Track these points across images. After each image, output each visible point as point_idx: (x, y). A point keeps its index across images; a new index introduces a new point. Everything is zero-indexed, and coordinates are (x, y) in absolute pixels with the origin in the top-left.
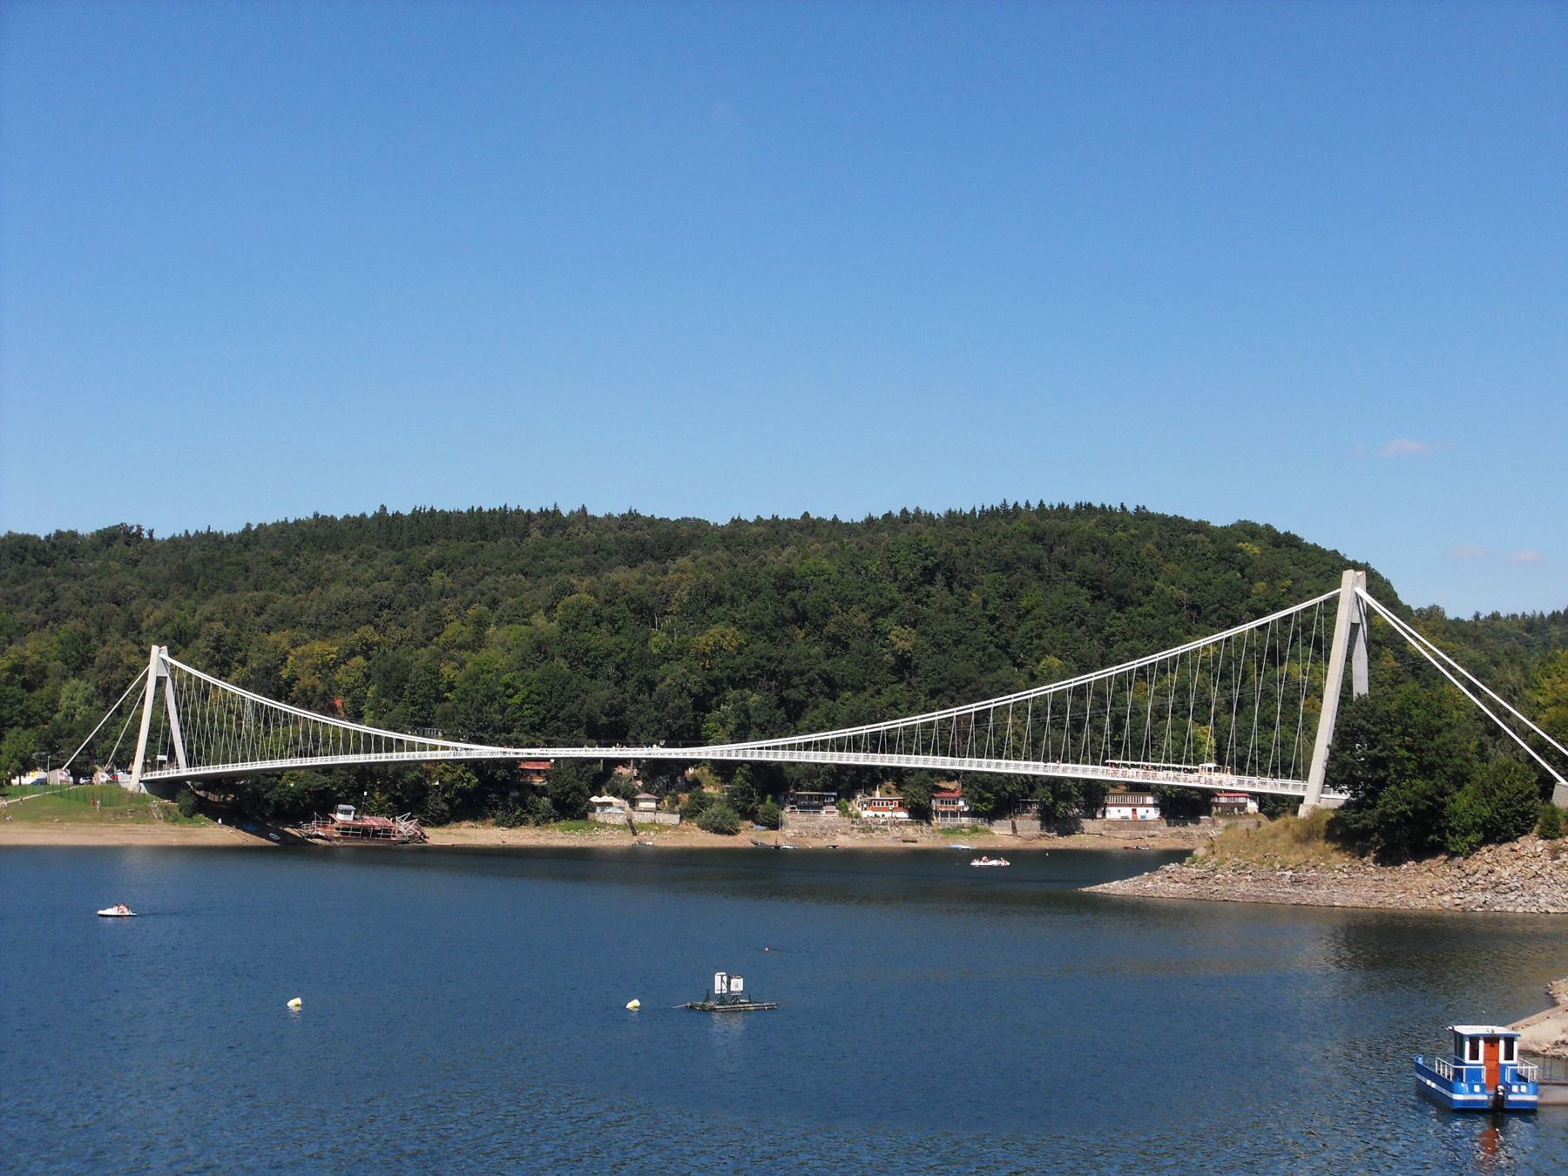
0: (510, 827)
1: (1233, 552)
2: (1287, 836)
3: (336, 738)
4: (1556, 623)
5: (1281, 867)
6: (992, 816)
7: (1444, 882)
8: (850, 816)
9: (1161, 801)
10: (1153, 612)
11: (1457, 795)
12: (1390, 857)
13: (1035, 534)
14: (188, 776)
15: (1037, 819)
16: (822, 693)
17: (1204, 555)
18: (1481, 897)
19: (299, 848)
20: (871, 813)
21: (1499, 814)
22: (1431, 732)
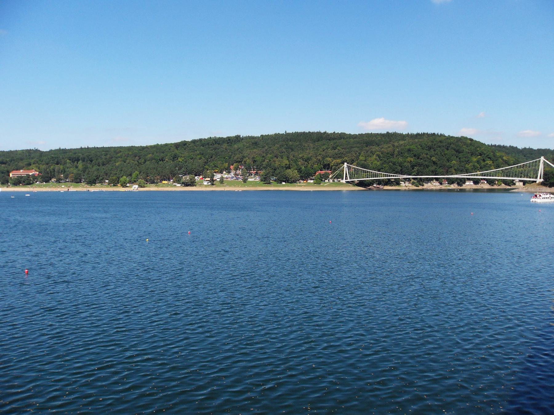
3: (375, 175)
14: (28, 192)
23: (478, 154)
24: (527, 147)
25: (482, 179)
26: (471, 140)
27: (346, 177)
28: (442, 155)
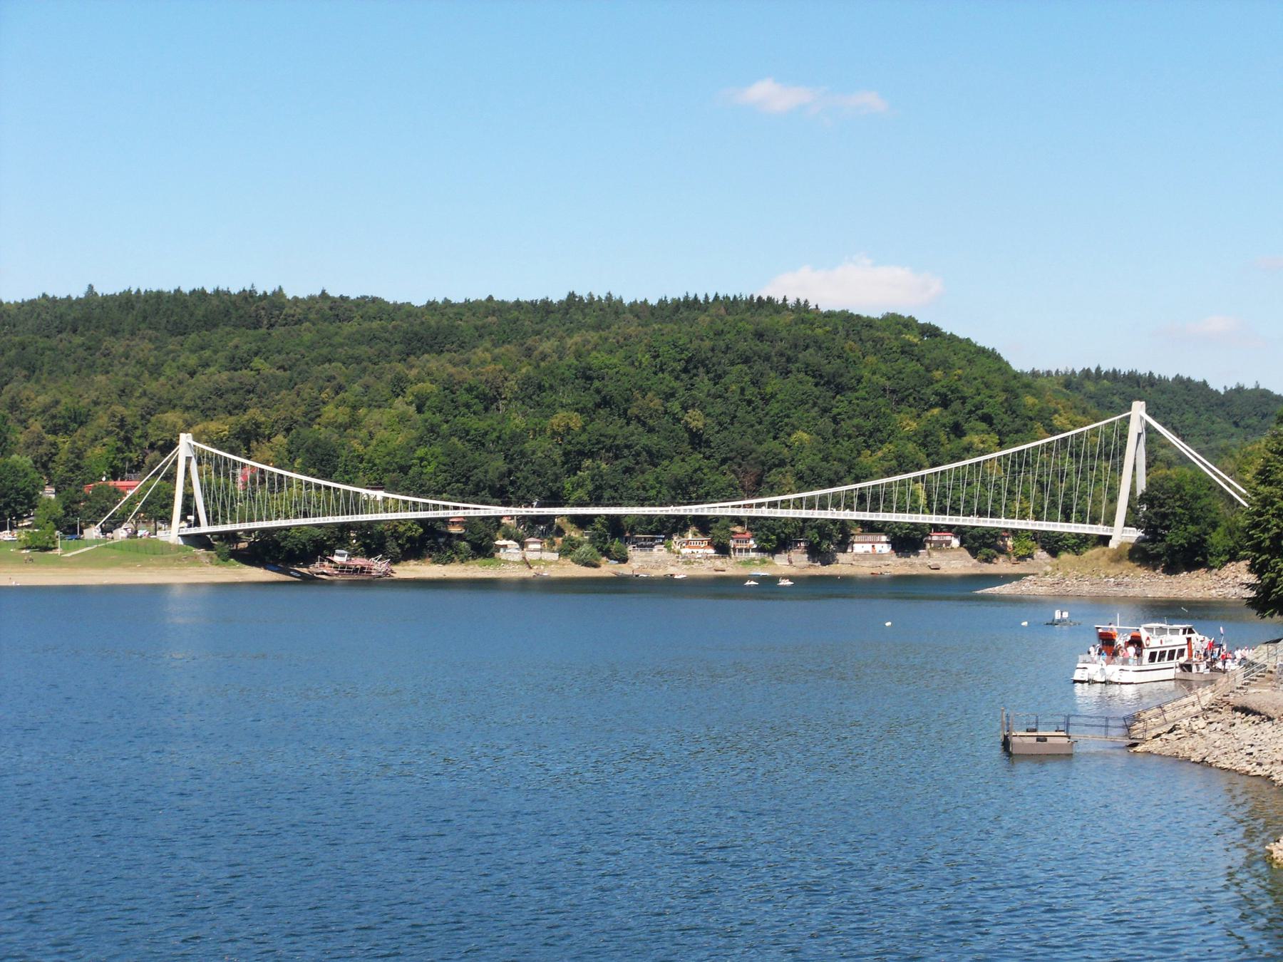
0: (444, 564)
1: (911, 346)
2: (1105, 558)
4: (1089, 379)
5: (1106, 576)
6: (773, 552)
7: (1209, 582)
8: (674, 552)
9: (892, 539)
10: (867, 396)
11: (1213, 535)
12: (1171, 570)
13: (756, 331)
15: (804, 553)
16: (646, 461)
17: (891, 349)
18: (1233, 591)
19: (309, 580)
20: (689, 551)
21: (1239, 545)
22: (1196, 498)
23: (933, 399)
24: (1250, 385)
25: (936, 528)
26: (931, 332)
27: (188, 508)
28: (749, 402)
